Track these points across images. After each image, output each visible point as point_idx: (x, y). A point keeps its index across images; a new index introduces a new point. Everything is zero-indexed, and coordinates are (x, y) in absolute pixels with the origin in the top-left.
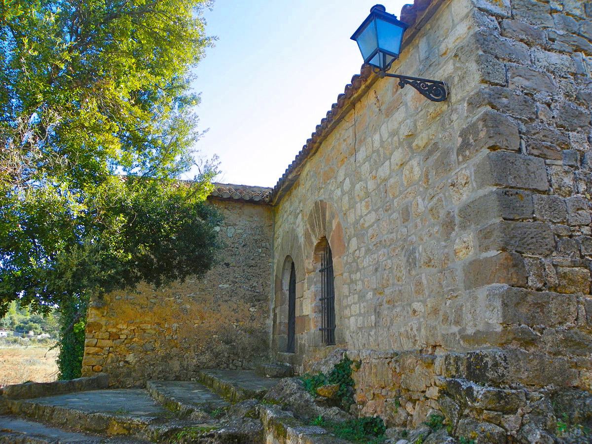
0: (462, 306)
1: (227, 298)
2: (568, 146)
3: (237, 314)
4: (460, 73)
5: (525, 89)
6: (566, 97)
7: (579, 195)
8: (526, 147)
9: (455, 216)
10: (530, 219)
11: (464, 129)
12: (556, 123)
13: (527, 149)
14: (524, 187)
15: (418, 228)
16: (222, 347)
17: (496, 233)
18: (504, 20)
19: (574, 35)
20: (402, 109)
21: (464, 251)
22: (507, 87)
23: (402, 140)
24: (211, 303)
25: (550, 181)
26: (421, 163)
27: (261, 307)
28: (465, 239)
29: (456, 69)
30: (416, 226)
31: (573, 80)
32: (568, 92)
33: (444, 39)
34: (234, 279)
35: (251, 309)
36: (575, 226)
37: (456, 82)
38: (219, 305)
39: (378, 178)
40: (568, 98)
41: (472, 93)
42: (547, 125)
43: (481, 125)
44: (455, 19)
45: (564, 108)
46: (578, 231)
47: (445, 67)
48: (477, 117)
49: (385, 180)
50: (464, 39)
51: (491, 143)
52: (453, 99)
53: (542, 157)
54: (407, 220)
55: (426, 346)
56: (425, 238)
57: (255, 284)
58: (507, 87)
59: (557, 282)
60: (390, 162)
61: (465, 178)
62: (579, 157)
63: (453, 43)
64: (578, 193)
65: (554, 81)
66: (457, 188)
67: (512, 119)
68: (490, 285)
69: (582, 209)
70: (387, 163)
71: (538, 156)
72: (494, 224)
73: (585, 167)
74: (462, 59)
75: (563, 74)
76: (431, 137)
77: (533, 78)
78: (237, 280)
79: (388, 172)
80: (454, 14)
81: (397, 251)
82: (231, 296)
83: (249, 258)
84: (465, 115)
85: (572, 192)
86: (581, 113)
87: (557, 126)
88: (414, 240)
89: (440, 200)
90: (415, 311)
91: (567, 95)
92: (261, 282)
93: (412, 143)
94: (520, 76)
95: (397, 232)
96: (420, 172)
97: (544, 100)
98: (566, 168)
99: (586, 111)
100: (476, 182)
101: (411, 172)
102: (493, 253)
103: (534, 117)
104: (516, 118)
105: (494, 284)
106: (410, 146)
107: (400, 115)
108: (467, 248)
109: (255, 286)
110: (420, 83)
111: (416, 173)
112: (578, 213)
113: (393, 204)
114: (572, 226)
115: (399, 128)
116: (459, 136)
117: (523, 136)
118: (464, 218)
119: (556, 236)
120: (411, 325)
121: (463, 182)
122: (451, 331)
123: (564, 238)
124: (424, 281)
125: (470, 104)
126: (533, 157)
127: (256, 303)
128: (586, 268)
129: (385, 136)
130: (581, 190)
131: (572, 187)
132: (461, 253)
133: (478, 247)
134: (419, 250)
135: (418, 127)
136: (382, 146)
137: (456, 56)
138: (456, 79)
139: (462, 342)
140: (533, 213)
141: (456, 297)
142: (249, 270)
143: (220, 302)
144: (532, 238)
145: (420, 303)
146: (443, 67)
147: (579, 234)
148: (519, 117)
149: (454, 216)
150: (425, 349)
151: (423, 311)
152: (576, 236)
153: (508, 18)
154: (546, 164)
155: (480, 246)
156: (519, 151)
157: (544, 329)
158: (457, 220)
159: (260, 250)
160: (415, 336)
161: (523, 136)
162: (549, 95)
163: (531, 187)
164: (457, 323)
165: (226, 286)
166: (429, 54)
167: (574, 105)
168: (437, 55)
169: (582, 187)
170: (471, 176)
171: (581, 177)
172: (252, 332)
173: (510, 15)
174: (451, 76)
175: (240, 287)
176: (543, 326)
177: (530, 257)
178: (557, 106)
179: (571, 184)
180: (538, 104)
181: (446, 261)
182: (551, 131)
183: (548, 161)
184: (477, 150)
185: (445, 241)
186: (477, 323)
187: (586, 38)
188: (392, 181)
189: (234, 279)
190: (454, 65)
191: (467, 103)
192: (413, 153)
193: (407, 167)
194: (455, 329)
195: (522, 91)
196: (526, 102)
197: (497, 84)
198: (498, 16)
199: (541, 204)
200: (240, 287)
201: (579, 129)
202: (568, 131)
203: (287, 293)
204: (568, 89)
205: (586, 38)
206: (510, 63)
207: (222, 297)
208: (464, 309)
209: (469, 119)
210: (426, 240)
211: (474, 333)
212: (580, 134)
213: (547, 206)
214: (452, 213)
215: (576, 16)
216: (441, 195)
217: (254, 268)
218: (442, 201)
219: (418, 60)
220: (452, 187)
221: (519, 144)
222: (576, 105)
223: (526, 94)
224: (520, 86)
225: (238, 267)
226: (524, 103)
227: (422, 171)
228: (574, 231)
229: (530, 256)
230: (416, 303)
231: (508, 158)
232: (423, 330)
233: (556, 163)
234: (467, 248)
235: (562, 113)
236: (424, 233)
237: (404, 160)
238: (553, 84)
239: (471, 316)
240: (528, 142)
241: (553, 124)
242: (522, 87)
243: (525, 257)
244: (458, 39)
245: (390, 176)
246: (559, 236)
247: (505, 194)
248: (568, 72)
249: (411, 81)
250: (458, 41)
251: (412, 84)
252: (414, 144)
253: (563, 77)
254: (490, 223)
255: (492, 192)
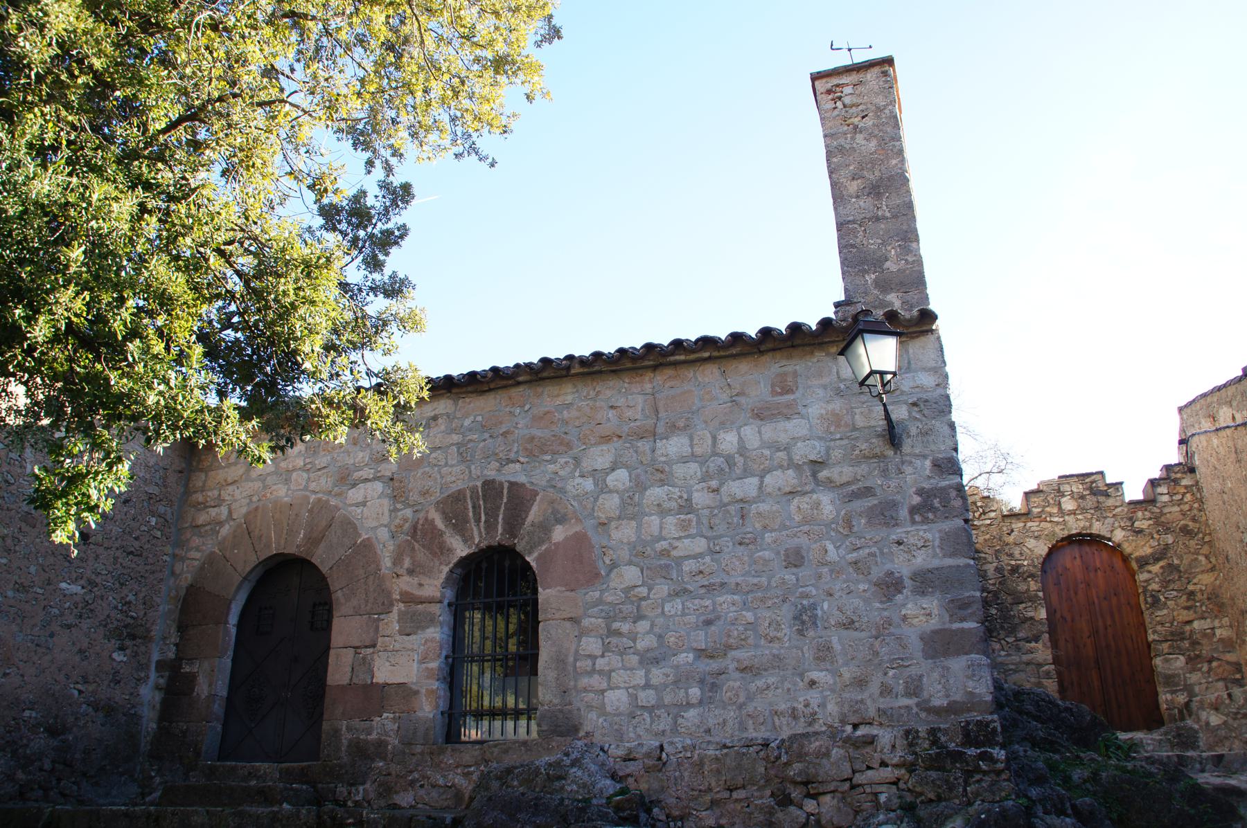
1: (71, 620)
3: (85, 662)
16: (40, 742)
24: (35, 625)
27: (136, 654)
34: (93, 577)
35: (115, 655)
38: (52, 635)
57: (131, 597)
78: (98, 580)
82: (80, 617)
83: (130, 533)
92: (143, 594)
105: (973, 655)
109: (130, 603)
127: (128, 643)
142: (126, 562)
143: (55, 627)
159: (153, 521)
165: (76, 589)
172: (108, 710)
175: (102, 598)
189: (93, 577)
200: (102, 598)
203: (233, 631)
207: (62, 615)
217: (136, 559)
225: (107, 548)
254: (967, 594)
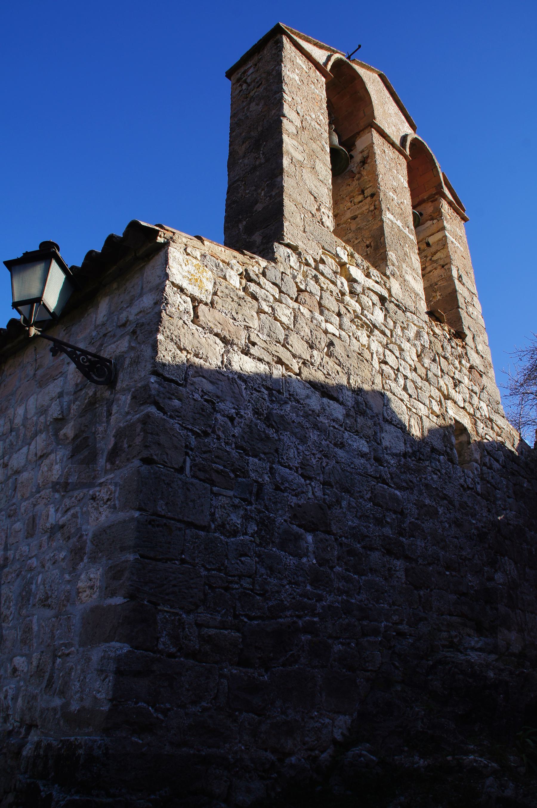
0: (71, 669)
2: (245, 474)
4: (133, 355)
5: (206, 394)
6: (254, 414)
7: (247, 537)
8: (191, 467)
9: (88, 541)
10: (177, 560)
11: (120, 427)
12: (236, 443)
13: (191, 470)
14: (176, 517)
15: (43, 548)
17: (127, 574)
18: (200, 304)
19: (278, 345)
20: (60, 381)
21: (88, 592)
22: (185, 386)
23: (48, 423)
25: (213, 515)
26: (65, 459)
28: (92, 576)
29: (131, 348)
30: (40, 546)
31: (266, 396)
32: (258, 409)
33: (127, 307)
36: (234, 576)
37: (126, 366)
39: (9, 467)
40: (256, 416)
41: (139, 385)
42: (223, 444)
43: (139, 427)
44: (144, 286)
45: (250, 427)
46: (237, 583)
47: (119, 342)
48: (138, 416)
49: (18, 472)
50: (147, 314)
51: (145, 454)
52: (119, 385)
53: (208, 483)
54: (32, 536)
55: (18, 724)
56: (48, 565)
58: (185, 386)
59: (197, 647)
60: (29, 449)
61: (109, 493)
62: (255, 490)
63: (136, 315)
64: (246, 534)
65: (244, 391)
66: (97, 504)
67: (181, 428)
68: (108, 645)
69: (245, 555)
70: (25, 450)
71: (204, 481)
72: (127, 561)
73: (260, 504)
74: (139, 338)
75: (256, 386)
76: (83, 428)
77: (220, 383)
79: (23, 462)
80: (145, 280)
81: (10, 577)
84: (126, 409)
85: (238, 532)
86: (268, 437)
87: (237, 447)
88: (34, 565)
89: (75, 516)
90: (15, 670)
91: (256, 412)
93: (61, 429)
94: (204, 377)
95: (17, 549)
96: (60, 473)
97: (226, 413)
98: (237, 501)
99: (275, 435)
100: (119, 500)
101: (50, 469)
102: (118, 600)
103: (209, 430)
104: (187, 429)
105: (113, 643)
106: (56, 434)
107: (54, 388)
108: (92, 587)
110: (80, 355)
111: (55, 472)
112: (240, 560)
113: (20, 509)
114: (230, 576)
115: (49, 406)
116: (114, 436)
117: (190, 452)
118: (97, 546)
119: (207, 587)
120: (6, 691)
121: (106, 498)
122: (53, 705)
123: (217, 590)
124: (35, 628)
125: (134, 397)
126: (197, 481)
128: (238, 631)
129: (32, 411)
130: (250, 531)
131: (239, 526)
132: (85, 594)
133: (104, 589)
134: (37, 581)
135: (72, 411)
136: (24, 425)
137: (134, 332)
138: (127, 361)
139: (62, 722)
140: (182, 553)
141: (68, 655)
144: (174, 586)
145: (24, 658)
146: (117, 341)
147: (236, 586)
148: (190, 427)
149: (85, 541)
150: (16, 730)
151: (25, 670)
152: (233, 589)
153: (206, 304)
154: (212, 492)
155: (106, 588)
156: (181, 470)
157: (169, 710)
158: (89, 547)
160: (8, 708)
161: (190, 452)
162: (234, 408)
163: (185, 519)
164: (62, 693)
166: (107, 320)
167: (261, 426)
168: (115, 324)
169: (253, 528)
170: (115, 492)
171: (253, 515)
173: (209, 301)
174: (123, 356)
176: (168, 706)
177: (167, 612)
178: (241, 422)
179: (239, 522)
180: (219, 416)
181: (65, 602)
182: (227, 452)
183: (215, 489)
184: (128, 460)
185: (70, 573)
186: (85, 697)
187: (290, 351)
188: (25, 475)
190: (130, 342)
191: (132, 395)
192: (58, 444)
193: (47, 462)
194: (57, 702)
195: (202, 397)
196: (203, 410)
197: (172, 381)
198: (194, 299)
199: (195, 543)
201: (262, 456)
202: (249, 456)
204: (259, 405)
205: (290, 351)
206: (195, 358)
208: (73, 674)
209: (129, 417)
210: (49, 568)
211: (79, 711)
212: (261, 462)
213: (203, 546)
214: (85, 537)
215: (284, 323)
216: (78, 509)
218: (77, 517)
219: (94, 323)
220: (92, 501)
221: (182, 460)
222: (264, 426)
223: (206, 400)
224: (200, 389)
226: (201, 411)
227: (62, 472)
228: (231, 582)
229: (166, 609)
230: (18, 658)
231: (163, 478)
232: (20, 700)
233: (224, 494)
234: (92, 587)
235: (245, 433)
236: (47, 557)
237: (45, 451)
238: (242, 396)
239: (78, 684)
240: (195, 460)
241: (231, 445)
242: (202, 391)
243: (160, 611)
244: (141, 312)
245: (24, 469)
246: (211, 587)
247: (150, 523)
248: (263, 385)
249: (69, 349)
250: (141, 315)
251: (70, 355)
252: (62, 432)
253: (255, 389)
255: (132, 519)
